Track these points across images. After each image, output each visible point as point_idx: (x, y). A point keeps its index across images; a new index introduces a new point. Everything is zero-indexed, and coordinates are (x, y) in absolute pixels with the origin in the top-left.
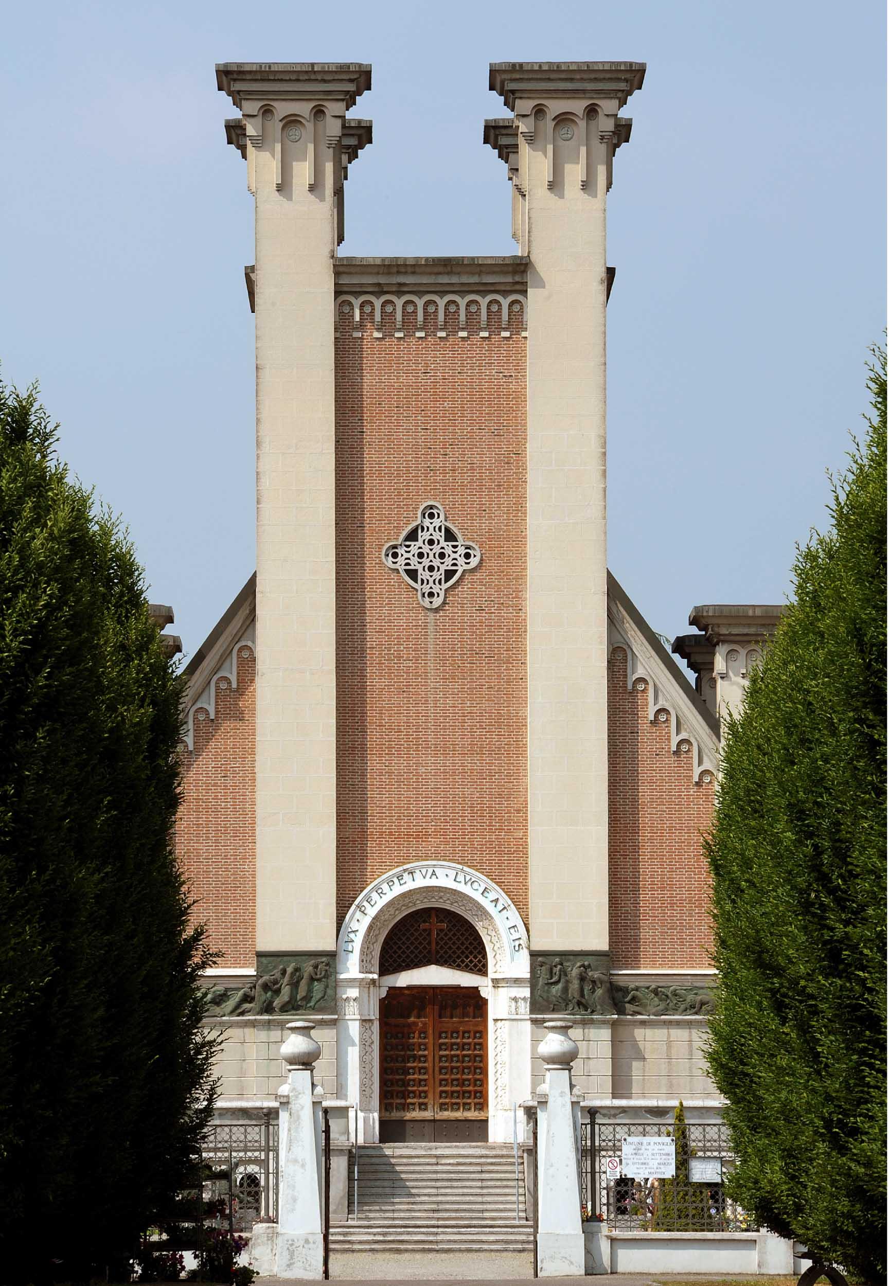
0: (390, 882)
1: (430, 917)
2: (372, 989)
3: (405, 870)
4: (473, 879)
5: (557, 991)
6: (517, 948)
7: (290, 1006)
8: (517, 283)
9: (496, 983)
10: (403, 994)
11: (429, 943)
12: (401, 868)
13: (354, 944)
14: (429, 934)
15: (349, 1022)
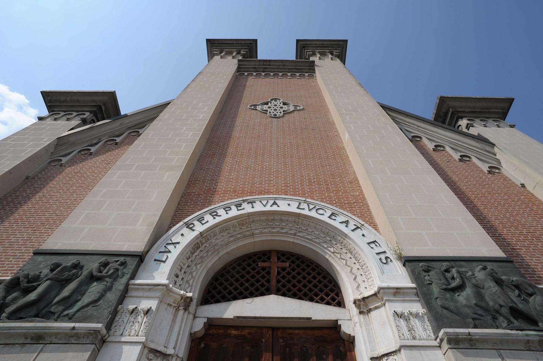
0: (227, 209)
1: (269, 258)
2: (181, 312)
3: (244, 201)
4: (317, 207)
5: (467, 299)
6: (384, 261)
7: (34, 311)
8: (310, 69)
9: (364, 305)
10: (229, 336)
11: (268, 281)
12: (241, 199)
13: (169, 255)
14: (269, 273)
15: (126, 348)
